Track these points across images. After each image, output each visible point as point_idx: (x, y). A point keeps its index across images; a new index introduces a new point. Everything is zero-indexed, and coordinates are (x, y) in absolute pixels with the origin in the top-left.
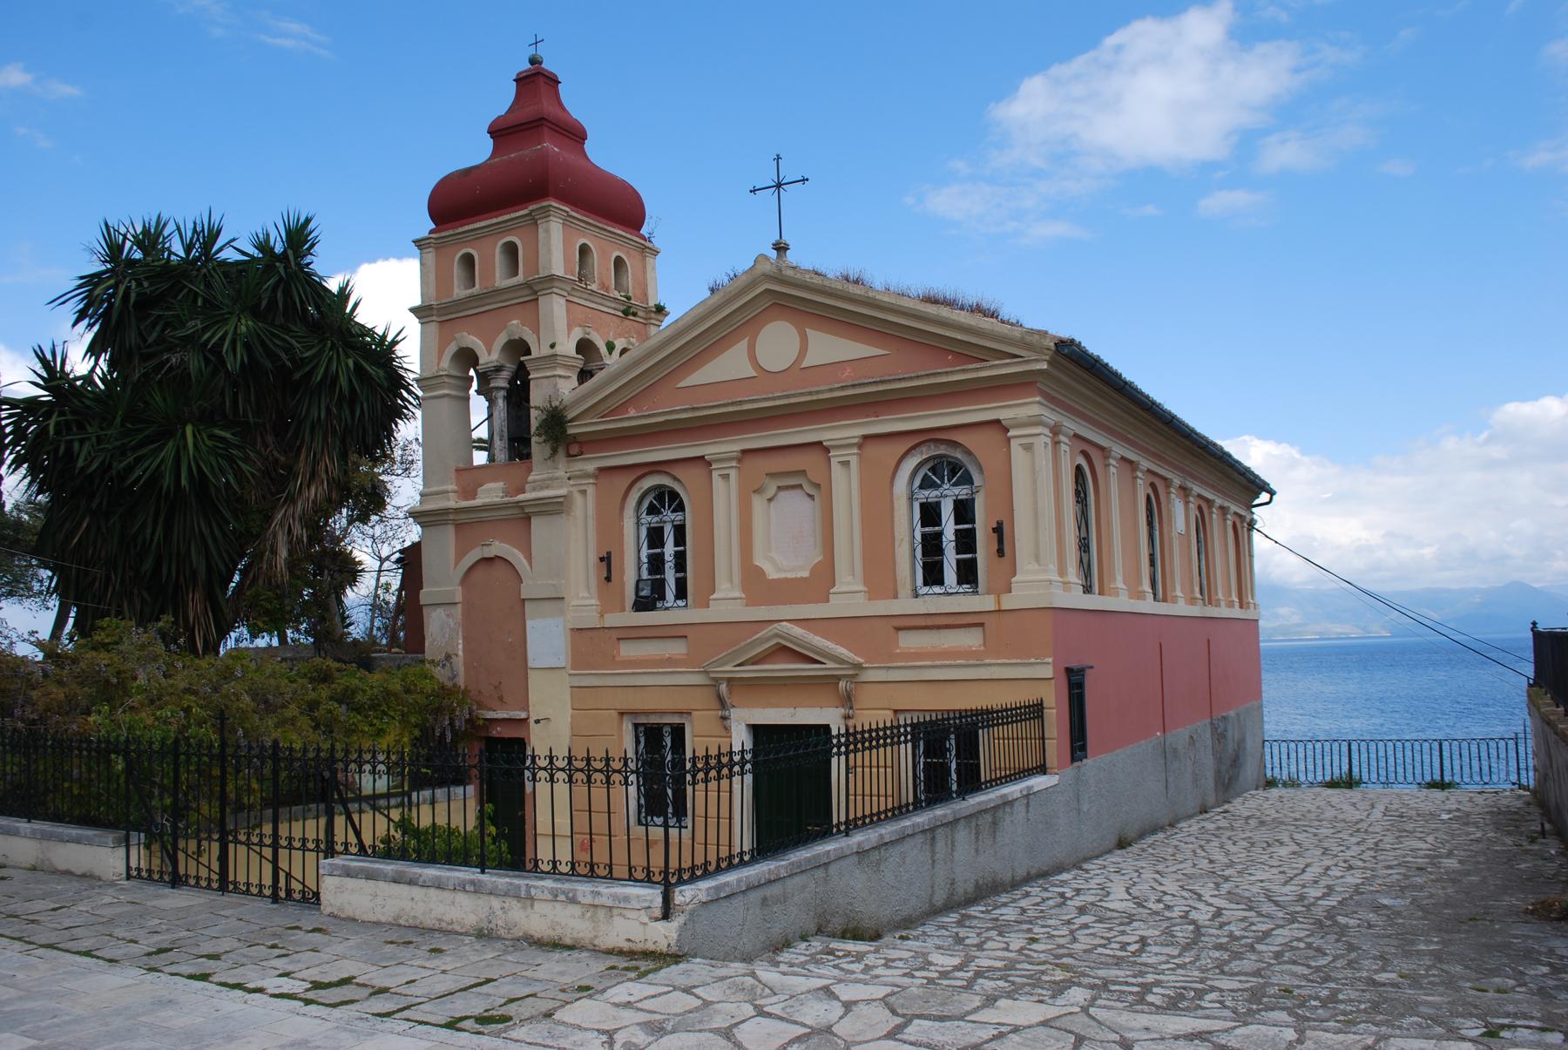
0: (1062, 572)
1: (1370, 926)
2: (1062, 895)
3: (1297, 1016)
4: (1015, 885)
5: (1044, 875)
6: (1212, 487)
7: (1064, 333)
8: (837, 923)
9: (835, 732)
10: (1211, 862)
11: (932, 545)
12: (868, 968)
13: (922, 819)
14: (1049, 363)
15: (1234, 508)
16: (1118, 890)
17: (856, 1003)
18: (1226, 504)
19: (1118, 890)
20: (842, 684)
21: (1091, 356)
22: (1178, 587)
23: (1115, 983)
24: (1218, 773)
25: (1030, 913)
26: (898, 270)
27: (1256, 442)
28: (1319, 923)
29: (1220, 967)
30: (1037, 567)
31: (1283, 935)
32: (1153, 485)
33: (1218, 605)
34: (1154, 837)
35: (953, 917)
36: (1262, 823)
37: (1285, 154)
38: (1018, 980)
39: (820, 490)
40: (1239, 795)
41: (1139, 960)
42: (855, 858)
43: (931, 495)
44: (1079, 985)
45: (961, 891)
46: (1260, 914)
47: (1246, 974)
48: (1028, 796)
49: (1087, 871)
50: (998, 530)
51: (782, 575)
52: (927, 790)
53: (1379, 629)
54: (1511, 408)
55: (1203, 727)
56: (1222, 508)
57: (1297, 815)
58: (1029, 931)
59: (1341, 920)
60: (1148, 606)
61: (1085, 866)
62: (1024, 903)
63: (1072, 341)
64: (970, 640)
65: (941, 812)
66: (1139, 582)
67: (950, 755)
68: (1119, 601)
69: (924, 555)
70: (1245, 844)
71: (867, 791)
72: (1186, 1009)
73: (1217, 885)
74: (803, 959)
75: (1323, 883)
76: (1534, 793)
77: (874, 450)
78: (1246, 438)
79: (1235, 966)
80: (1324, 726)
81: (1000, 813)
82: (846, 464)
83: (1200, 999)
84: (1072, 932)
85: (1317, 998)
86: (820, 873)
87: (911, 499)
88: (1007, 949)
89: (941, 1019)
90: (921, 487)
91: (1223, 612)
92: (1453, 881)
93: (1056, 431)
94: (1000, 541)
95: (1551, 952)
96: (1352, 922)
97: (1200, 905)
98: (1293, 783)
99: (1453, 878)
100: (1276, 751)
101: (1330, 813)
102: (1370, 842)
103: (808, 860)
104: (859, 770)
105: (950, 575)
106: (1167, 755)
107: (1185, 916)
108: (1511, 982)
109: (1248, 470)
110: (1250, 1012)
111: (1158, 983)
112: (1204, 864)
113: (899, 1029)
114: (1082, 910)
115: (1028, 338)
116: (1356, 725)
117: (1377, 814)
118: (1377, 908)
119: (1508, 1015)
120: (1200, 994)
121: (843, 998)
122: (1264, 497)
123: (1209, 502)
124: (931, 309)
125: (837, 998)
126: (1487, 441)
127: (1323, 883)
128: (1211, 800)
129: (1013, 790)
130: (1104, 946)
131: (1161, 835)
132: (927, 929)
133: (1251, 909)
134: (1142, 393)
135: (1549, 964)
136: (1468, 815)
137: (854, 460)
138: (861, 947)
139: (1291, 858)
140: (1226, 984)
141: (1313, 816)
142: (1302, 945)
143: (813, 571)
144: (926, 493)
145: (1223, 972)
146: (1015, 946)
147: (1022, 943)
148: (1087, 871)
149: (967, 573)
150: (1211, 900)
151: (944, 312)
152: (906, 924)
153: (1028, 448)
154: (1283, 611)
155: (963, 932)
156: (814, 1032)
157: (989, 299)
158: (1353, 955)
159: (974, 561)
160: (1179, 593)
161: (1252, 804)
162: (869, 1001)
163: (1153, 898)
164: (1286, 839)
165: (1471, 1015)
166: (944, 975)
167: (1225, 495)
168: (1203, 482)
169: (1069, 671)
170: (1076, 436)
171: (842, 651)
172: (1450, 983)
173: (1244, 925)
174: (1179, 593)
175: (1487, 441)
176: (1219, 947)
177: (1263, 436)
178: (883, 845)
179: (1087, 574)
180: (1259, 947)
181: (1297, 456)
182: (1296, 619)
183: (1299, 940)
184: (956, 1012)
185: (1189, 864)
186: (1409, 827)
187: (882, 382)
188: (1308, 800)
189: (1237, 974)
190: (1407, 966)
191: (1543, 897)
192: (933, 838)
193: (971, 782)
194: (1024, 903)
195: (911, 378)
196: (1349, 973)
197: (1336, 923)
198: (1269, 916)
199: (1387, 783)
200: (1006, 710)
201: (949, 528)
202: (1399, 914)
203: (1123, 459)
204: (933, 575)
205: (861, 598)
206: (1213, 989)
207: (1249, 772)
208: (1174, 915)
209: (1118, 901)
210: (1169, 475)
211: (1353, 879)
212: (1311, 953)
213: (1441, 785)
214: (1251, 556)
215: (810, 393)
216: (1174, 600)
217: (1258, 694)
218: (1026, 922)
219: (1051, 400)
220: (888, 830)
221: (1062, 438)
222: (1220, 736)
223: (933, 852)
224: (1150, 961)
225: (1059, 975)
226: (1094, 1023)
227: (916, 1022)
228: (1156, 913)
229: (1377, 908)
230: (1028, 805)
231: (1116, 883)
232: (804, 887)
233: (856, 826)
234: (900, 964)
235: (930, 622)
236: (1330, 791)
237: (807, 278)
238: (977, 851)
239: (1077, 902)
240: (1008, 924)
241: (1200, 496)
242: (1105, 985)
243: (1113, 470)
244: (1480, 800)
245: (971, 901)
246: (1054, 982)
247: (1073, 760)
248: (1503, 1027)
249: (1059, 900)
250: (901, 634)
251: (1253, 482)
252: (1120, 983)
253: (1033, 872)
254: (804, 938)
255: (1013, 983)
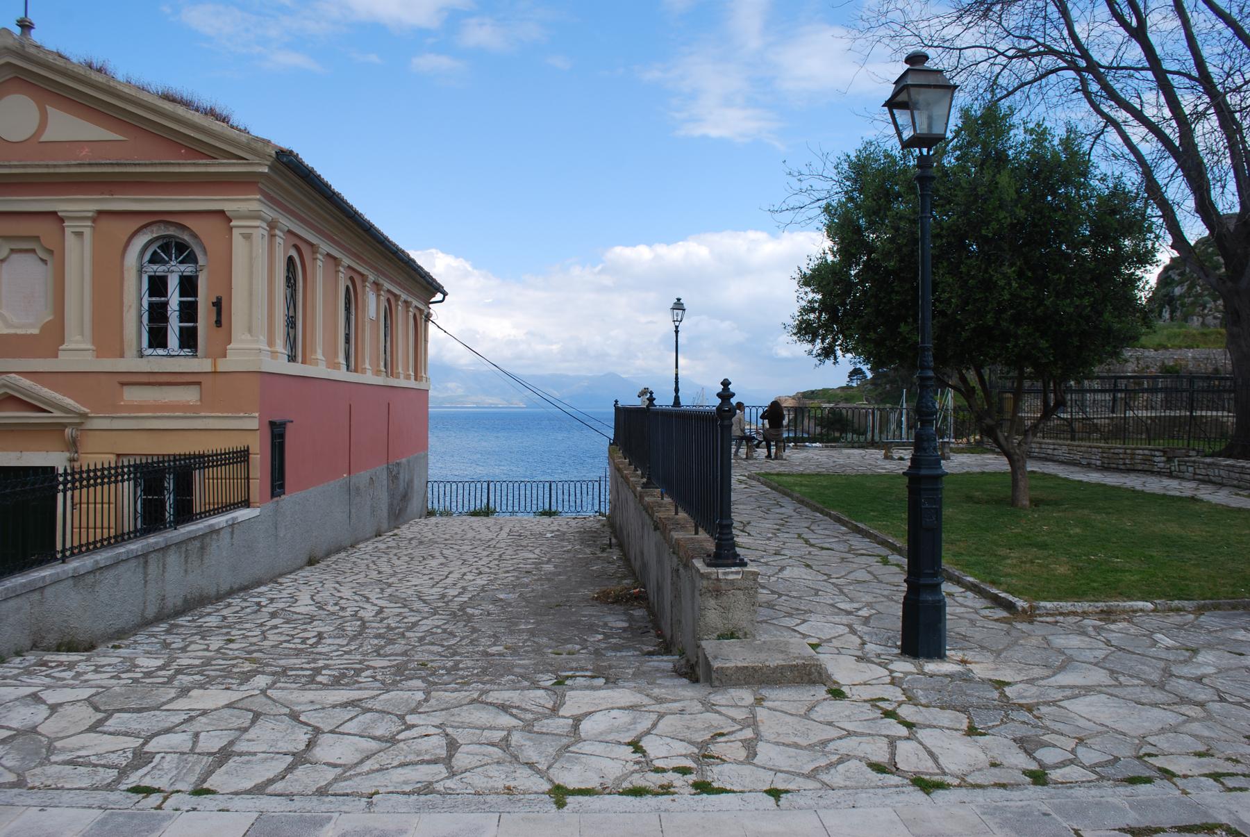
0: (271, 343)
1: (489, 614)
2: (258, 604)
3: (429, 682)
4: (219, 598)
5: (244, 588)
6: (399, 284)
7: (285, 145)
8: (52, 639)
9: (61, 471)
10: (380, 573)
11: (158, 314)
12: (78, 674)
13: (136, 546)
14: (270, 167)
15: (415, 303)
16: (304, 598)
17: (61, 705)
18: (410, 299)
19: (304, 598)
20: (68, 431)
21: (306, 167)
22: (367, 361)
23: (292, 669)
24: (391, 506)
25: (230, 620)
26: (140, 66)
27: (441, 255)
28: (454, 614)
29: (378, 652)
30: (249, 337)
31: (427, 624)
32: (352, 279)
33: (398, 377)
34: (337, 556)
35: (164, 626)
36: (421, 543)
37: (480, 34)
38: (213, 673)
39: (54, 256)
40: (406, 522)
41: (315, 650)
42: (71, 582)
43: (159, 269)
44: (263, 673)
45: (170, 605)
46: (412, 610)
47: (397, 655)
48: (233, 525)
49: (281, 584)
50: (218, 304)
51: (12, 331)
52: (143, 522)
53: (518, 402)
54: (619, 251)
55: (381, 472)
56: (406, 302)
57: (447, 536)
58: (228, 633)
59: (469, 611)
60: (342, 374)
61: (280, 580)
62: (225, 612)
63: (291, 152)
64: (189, 396)
65: (154, 540)
66: (336, 355)
67: (167, 491)
68: (319, 370)
69: (151, 320)
70: (407, 559)
71: (84, 524)
72: (346, 685)
73: (382, 590)
74: (16, 671)
75: (459, 585)
76: (608, 518)
77: (105, 224)
78: (433, 251)
79: (389, 650)
80: (481, 472)
81: (208, 540)
82: (79, 234)
83: (358, 675)
84: (263, 632)
85: (444, 668)
86: (36, 596)
87: (140, 271)
88: (207, 650)
89: (140, 710)
90: (152, 261)
91: (401, 382)
92: (549, 580)
93: (272, 225)
94: (219, 313)
95: (606, 624)
96: (477, 612)
97: (367, 606)
98: (447, 513)
99: (549, 578)
100: (436, 489)
101: (470, 534)
102: (496, 555)
103: (24, 585)
104: (84, 506)
105: (173, 340)
106: (351, 491)
107: (355, 614)
108: (578, 647)
109: (427, 274)
110: (395, 683)
111: (326, 667)
112: (374, 575)
113: (100, 722)
114: (273, 615)
115: (254, 145)
116: (497, 471)
117: (504, 534)
118: (495, 601)
119: (572, 669)
120: (358, 672)
121: (50, 701)
122: (439, 296)
123: (397, 297)
124: (168, 106)
125: (44, 702)
126: (600, 272)
127: (459, 585)
128: (385, 526)
129: (220, 520)
130: (288, 642)
131: (343, 554)
132: (138, 638)
133: (405, 606)
134: (346, 203)
135: (604, 633)
136: (564, 534)
137: (87, 232)
138: (74, 657)
139: (443, 565)
140: (379, 663)
141: (458, 537)
142: (439, 631)
143: (43, 329)
144: (155, 267)
145: (379, 655)
146: (214, 647)
147: (221, 644)
148: (281, 584)
149: (189, 339)
150: (376, 602)
151: (181, 111)
152: (118, 636)
153: (247, 237)
154: (451, 385)
155: (169, 639)
156: (19, 733)
157: (221, 106)
158: (475, 635)
159: (195, 329)
160: (367, 366)
161: (415, 529)
162: (73, 703)
163: (332, 602)
164: (437, 554)
165: (548, 671)
166: (148, 674)
167: (409, 292)
168: (392, 281)
169: (272, 424)
170: (290, 232)
171: (69, 402)
172: (538, 650)
173: (398, 619)
174: (367, 366)
175: (600, 272)
176: (378, 636)
177: (446, 252)
178: (98, 569)
179: (293, 346)
180: (408, 634)
181: (470, 269)
182: (460, 392)
183: (438, 627)
184: (153, 704)
185: (363, 575)
186: (524, 543)
187: (118, 164)
188: (455, 525)
189: (391, 655)
190: (510, 641)
191: (604, 588)
192: (146, 562)
193: (185, 513)
194: (225, 612)
195: (146, 165)
196: (470, 649)
197: (466, 613)
198: (418, 611)
199: (513, 513)
200: (217, 455)
201: (174, 299)
202: (509, 604)
203: (328, 255)
204: (158, 339)
205: (89, 356)
206: (368, 668)
207: (415, 504)
208: (347, 614)
209: (304, 605)
210: (366, 272)
211: (481, 581)
212: (445, 636)
213: (549, 513)
214: (426, 341)
215: (47, 166)
216: (364, 371)
217: (425, 447)
218: (226, 627)
219: (271, 200)
220: (103, 557)
221: (277, 232)
222: (394, 478)
223: (146, 574)
224: (324, 650)
225: (247, 667)
226: (270, 702)
227: (117, 715)
228: (333, 614)
229: (495, 601)
230: (232, 533)
231: (303, 593)
232: (19, 609)
233: (73, 554)
234: (109, 669)
235: (152, 379)
236: (473, 519)
237: (50, 58)
238: (186, 571)
239: (271, 609)
240: (210, 629)
241: (389, 291)
242: (285, 670)
243: (319, 263)
244: (573, 523)
245: (179, 613)
246: (243, 673)
247: (273, 496)
248: (567, 678)
249: (256, 608)
250: (126, 390)
251: (431, 284)
252: (297, 669)
253: (236, 586)
254: (18, 654)
255: (208, 676)
